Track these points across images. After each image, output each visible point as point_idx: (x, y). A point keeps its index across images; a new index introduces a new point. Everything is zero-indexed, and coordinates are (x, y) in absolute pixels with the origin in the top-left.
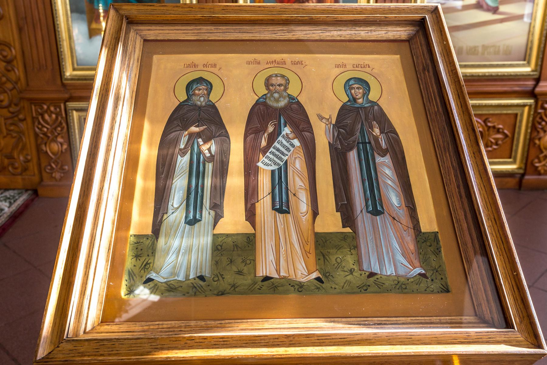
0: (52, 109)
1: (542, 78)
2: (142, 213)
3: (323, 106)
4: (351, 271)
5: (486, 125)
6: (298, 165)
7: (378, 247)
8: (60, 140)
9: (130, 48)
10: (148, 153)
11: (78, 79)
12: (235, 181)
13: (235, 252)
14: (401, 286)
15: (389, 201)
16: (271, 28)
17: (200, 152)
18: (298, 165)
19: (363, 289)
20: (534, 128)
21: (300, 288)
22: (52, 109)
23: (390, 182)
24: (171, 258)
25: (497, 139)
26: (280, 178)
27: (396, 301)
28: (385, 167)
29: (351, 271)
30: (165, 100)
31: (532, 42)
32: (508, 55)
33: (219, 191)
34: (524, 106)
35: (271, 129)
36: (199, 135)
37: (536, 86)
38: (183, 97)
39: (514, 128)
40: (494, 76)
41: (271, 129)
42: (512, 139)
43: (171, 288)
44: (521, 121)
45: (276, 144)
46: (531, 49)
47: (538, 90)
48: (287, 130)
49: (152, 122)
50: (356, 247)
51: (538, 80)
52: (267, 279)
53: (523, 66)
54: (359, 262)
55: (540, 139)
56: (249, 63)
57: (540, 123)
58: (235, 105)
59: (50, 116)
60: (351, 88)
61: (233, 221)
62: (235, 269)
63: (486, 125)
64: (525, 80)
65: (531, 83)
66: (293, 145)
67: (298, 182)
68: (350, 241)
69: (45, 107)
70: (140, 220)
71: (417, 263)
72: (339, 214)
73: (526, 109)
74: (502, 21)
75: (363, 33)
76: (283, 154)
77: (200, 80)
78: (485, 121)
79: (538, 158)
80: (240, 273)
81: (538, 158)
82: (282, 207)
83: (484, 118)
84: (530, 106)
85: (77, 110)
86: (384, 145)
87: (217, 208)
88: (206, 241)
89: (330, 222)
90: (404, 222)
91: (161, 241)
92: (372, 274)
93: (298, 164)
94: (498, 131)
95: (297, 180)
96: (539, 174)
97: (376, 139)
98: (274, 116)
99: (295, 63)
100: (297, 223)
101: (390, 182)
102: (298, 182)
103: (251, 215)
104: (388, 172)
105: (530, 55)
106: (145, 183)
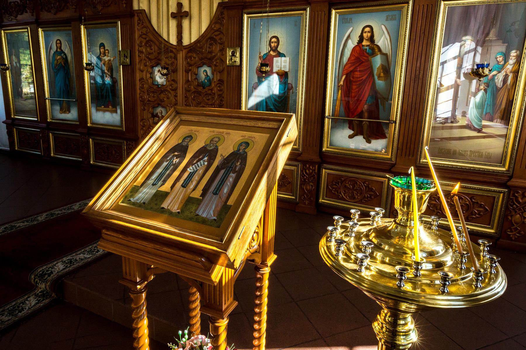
0: (311, 167)
1: (514, 176)
2: (142, 179)
3: (225, 150)
4: (191, 212)
5: (472, 201)
6: (200, 172)
7: (207, 206)
8: (311, 184)
9: (173, 122)
10: (157, 159)
11: (365, 157)
12: (176, 173)
13: (161, 196)
14: (204, 221)
15: (224, 190)
16: (225, 119)
17: (173, 162)
18: (200, 172)
19: (191, 219)
20: (507, 208)
21: (170, 213)
22: (311, 167)
23: (229, 184)
24: (140, 195)
25: (480, 211)
26: (191, 175)
27: (204, 227)
28: (233, 175)
29: (191, 212)
30: (173, 142)
31: (506, 152)
32: (489, 159)
33: (169, 176)
34: (500, 192)
35: (201, 157)
36: (176, 156)
37: (509, 180)
38: (180, 142)
39: (492, 206)
40: (458, 168)
41: (201, 157)
42: (491, 212)
43: (134, 204)
44: (498, 202)
45: (199, 163)
46: (506, 157)
47: (509, 183)
48: (206, 158)
49: (165, 149)
50: (199, 204)
51: (511, 177)
52: (163, 208)
53: (500, 167)
54: (196, 210)
55: (512, 216)
56: (210, 132)
57: (512, 206)
58: (194, 148)
59: (309, 171)
60: (241, 145)
61: (166, 187)
62: (156, 202)
63: (472, 201)
64: (502, 176)
65: (506, 178)
66: (204, 164)
67: (196, 178)
68: (197, 202)
69: (308, 166)
70: (140, 180)
71: (216, 215)
72: (202, 192)
73: (502, 195)
74: (484, 137)
75: (260, 124)
76: (199, 167)
77: (191, 136)
78: (471, 199)
79: (510, 228)
80: (156, 204)
81: (510, 228)
82: (184, 186)
83: (470, 196)
84: (504, 193)
85: (325, 169)
86: (237, 169)
87: (164, 181)
88: (154, 191)
89: (197, 195)
90: (223, 200)
91: (141, 189)
92: (198, 215)
93: (201, 172)
94: (481, 206)
95: (197, 177)
96: (512, 240)
97: (236, 166)
98: (208, 152)
99: (227, 133)
100: (186, 192)
101: (229, 184)
102: (196, 178)
103: (204, 194)
104: (231, 180)
105: (505, 161)
106: (149, 169)
